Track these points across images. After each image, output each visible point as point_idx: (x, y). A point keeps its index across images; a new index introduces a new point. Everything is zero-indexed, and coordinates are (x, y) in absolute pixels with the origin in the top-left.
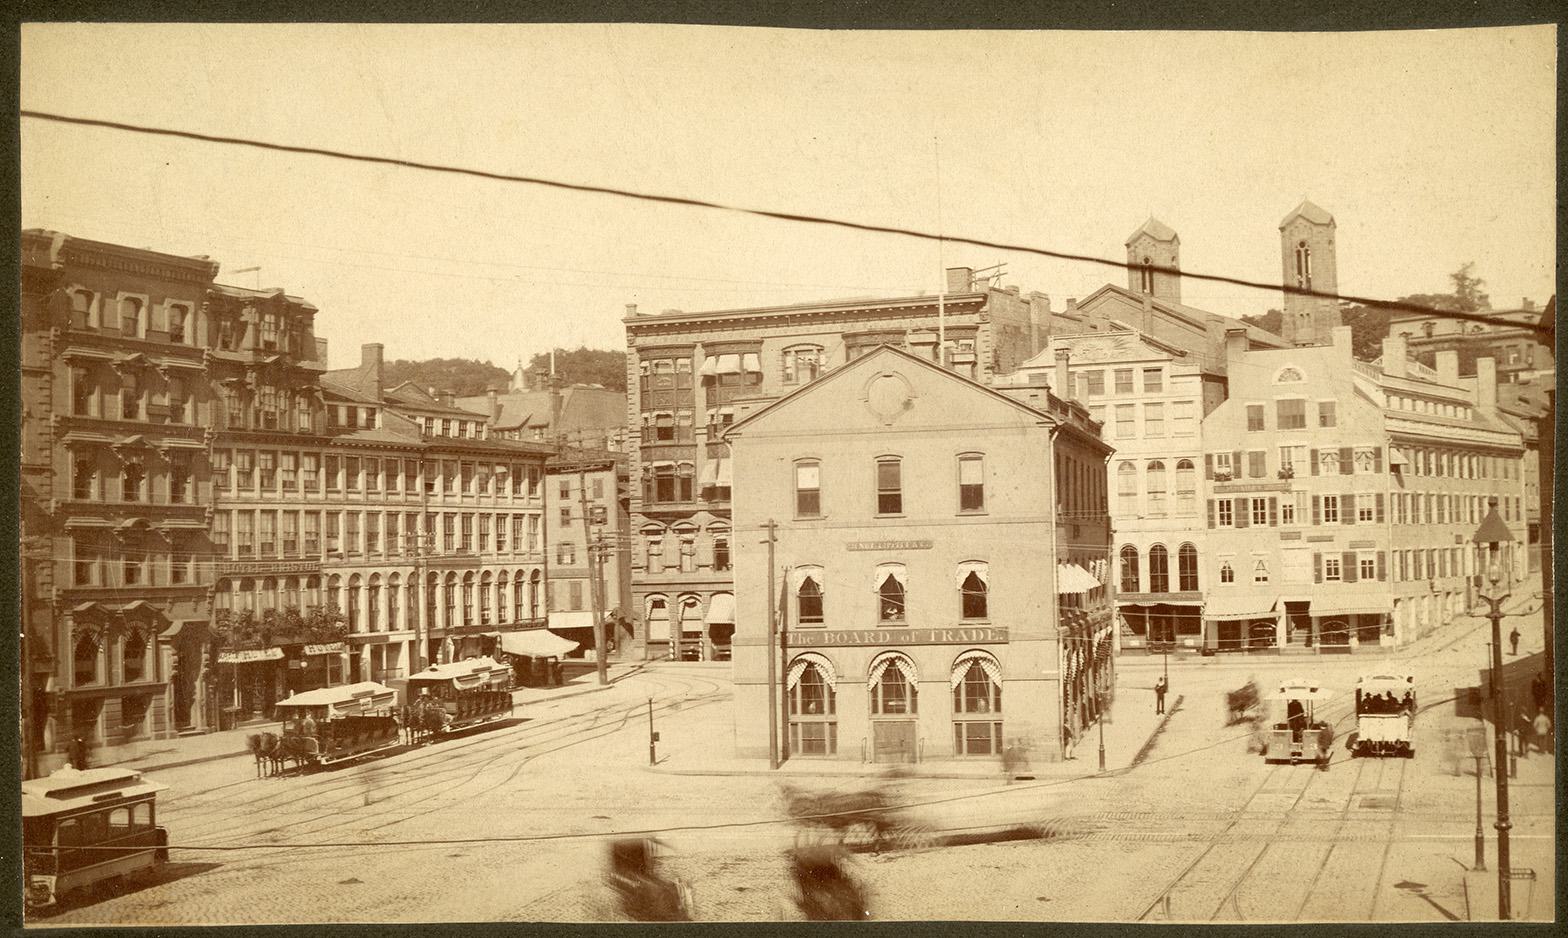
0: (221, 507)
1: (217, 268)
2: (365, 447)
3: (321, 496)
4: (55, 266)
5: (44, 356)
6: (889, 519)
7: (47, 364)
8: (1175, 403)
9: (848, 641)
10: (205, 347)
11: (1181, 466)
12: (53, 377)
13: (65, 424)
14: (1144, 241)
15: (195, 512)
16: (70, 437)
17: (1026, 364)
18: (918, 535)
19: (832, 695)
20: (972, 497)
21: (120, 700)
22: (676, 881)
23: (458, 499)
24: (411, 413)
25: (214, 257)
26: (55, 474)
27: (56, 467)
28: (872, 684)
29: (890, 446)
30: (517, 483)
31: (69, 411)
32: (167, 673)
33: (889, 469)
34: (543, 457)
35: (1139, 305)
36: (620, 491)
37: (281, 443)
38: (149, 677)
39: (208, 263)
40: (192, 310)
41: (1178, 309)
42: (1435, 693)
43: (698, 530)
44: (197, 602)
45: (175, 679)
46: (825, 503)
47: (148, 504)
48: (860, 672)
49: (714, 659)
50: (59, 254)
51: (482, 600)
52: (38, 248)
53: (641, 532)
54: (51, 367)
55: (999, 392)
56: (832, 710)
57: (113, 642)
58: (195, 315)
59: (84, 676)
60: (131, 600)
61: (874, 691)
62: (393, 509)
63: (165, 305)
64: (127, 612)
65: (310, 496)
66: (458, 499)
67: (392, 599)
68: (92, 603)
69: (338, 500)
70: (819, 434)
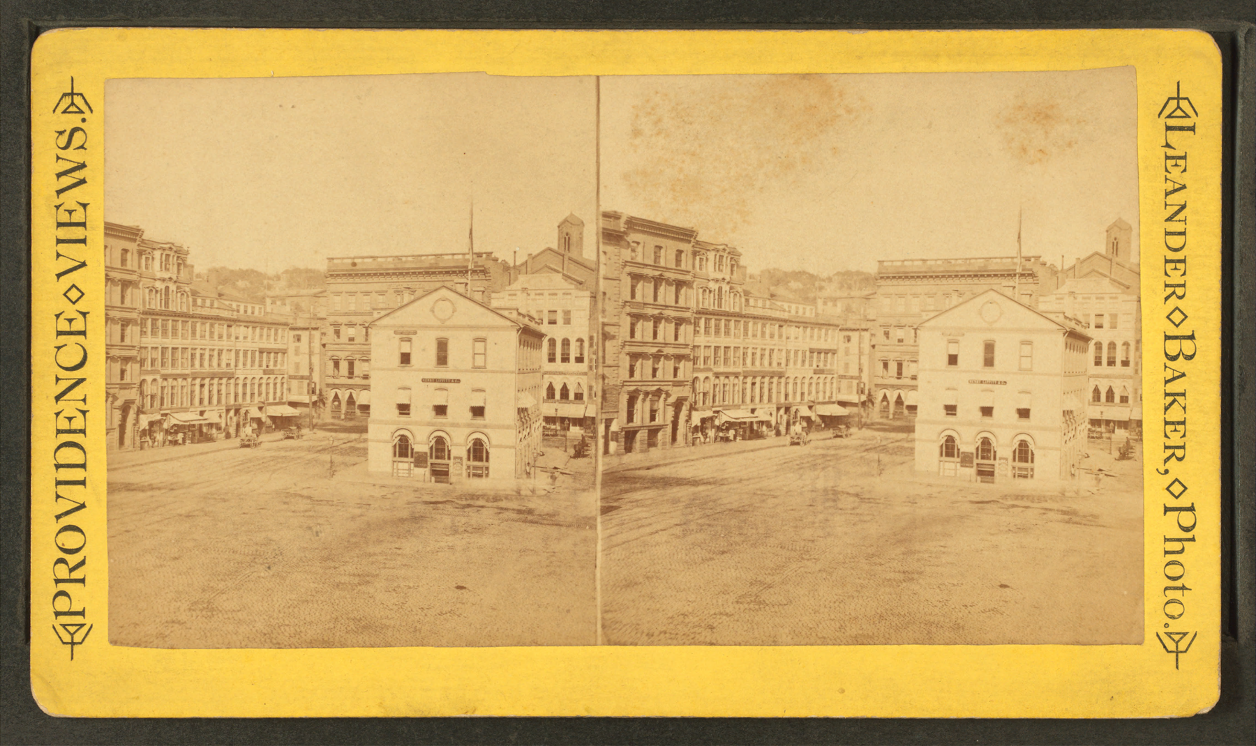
0: (142, 345)
4: (622, 230)
6: (988, 369)
17: (507, 288)
18: (1002, 378)
19: (1033, 454)
20: (953, 360)
22: (417, 526)
25: (141, 227)
28: (431, 445)
29: (989, 336)
33: (989, 348)
41: (580, 260)
42: (133, 471)
51: (201, 392)
56: (1032, 461)
59: (630, 418)
61: (1014, 452)
66: (216, 342)
67: (275, 388)
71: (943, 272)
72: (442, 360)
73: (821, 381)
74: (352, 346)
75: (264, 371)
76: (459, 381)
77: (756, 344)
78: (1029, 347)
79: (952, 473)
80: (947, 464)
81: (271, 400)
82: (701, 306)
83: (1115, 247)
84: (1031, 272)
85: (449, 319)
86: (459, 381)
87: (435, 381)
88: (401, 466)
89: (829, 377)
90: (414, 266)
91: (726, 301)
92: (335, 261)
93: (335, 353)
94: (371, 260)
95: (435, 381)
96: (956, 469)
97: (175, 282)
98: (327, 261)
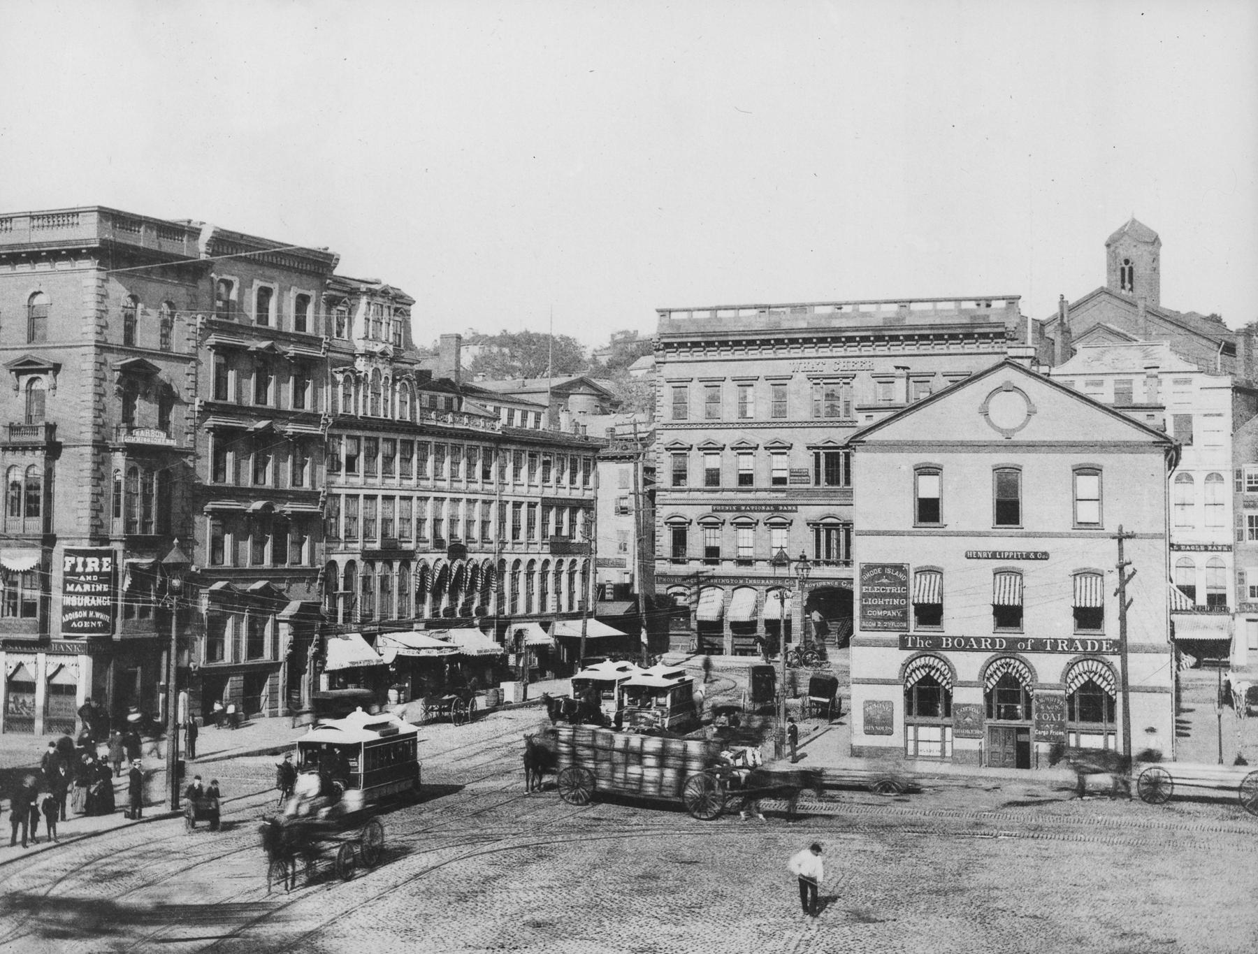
1: (338, 259)
2: (451, 436)
3: (413, 482)
4: (203, 257)
5: (192, 343)
7: (194, 351)
8: (1205, 415)
9: (965, 644)
10: (324, 337)
11: (1209, 477)
12: (199, 363)
13: (207, 409)
14: (1127, 241)
15: (312, 497)
16: (210, 422)
21: (242, 678)
23: (525, 489)
24: (483, 402)
26: (199, 458)
27: (199, 450)
30: (406, 460)
31: (210, 398)
32: (284, 652)
34: (596, 449)
35: (1132, 309)
36: (646, 482)
37: (384, 430)
38: (267, 655)
39: (327, 254)
40: (236, 285)
43: (757, 524)
44: (310, 584)
45: (290, 658)
46: (948, 512)
47: (310, 489)
48: (974, 676)
49: (734, 654)
50: (208, 245)
52: (189, 236)
53: (666, 523)
54: (196, 354)
55: (1117, 411)
57: (239, 619)
58: (317, 306)
60: (254, 581)
62: (472, 497)
63: (292, 292)
64: (253, 591)
65: (405, 482)
68: (225, 583)
69: (374, 484)
70: (942, 446)
71: (807, 330)
72: (1008, 512)
73: (565, 567)
74: (717, 495)
75: (552, 544)
76: (1045, 556)
77: (475, 493)
78: (1094, 480)
79: (935, 749)
80: (921, 729)
81: (565, 609)
82: (340, 411)
83: (1127, 274)
84: (1000, 330)
85: (1023, 426)
86: (1045, 556)
87: (994, 556)
88: (924, 733)
89: (580, 561)
90: (852, 323)
91: (386, 400)
92: (674, 316)
93: (681, 510)
94: (755, 312)
95: (994, 556)
96: (943, 741)
97: (392, 360)
98: (657, 315)
